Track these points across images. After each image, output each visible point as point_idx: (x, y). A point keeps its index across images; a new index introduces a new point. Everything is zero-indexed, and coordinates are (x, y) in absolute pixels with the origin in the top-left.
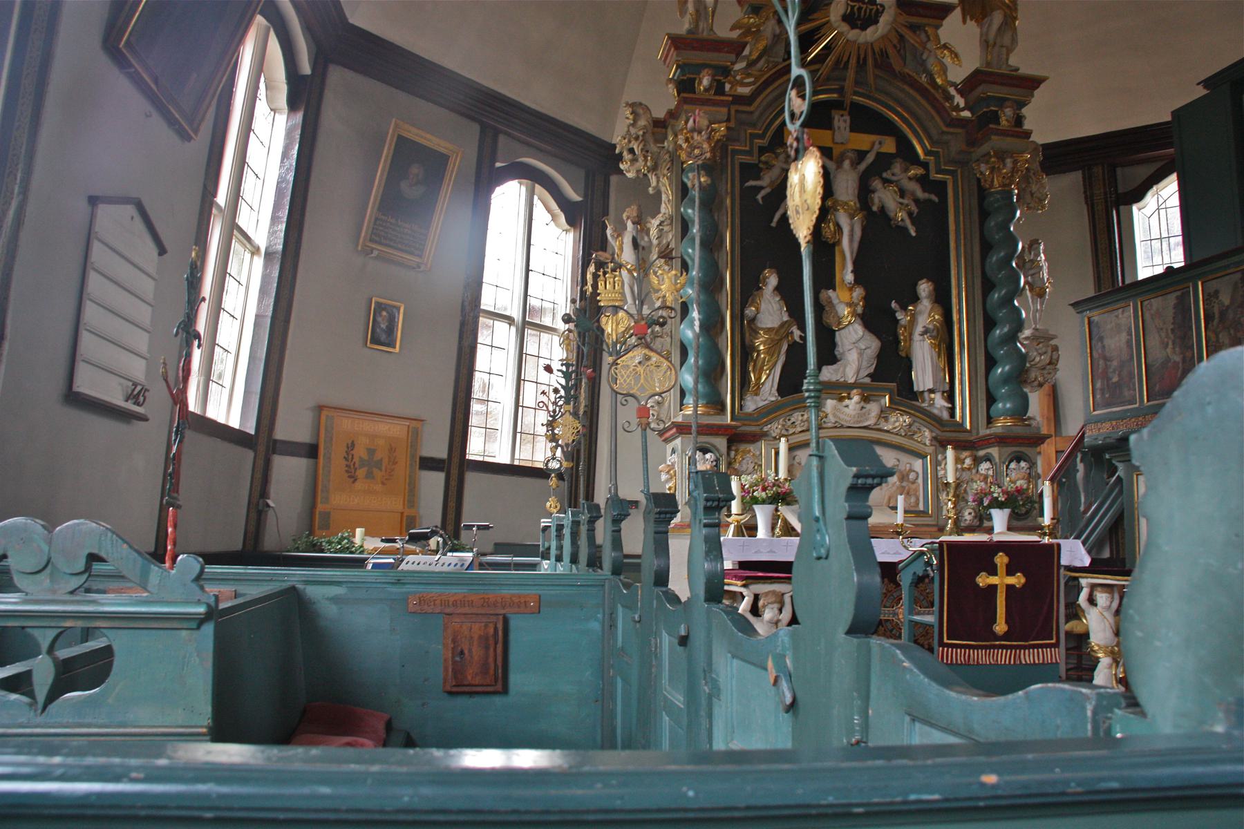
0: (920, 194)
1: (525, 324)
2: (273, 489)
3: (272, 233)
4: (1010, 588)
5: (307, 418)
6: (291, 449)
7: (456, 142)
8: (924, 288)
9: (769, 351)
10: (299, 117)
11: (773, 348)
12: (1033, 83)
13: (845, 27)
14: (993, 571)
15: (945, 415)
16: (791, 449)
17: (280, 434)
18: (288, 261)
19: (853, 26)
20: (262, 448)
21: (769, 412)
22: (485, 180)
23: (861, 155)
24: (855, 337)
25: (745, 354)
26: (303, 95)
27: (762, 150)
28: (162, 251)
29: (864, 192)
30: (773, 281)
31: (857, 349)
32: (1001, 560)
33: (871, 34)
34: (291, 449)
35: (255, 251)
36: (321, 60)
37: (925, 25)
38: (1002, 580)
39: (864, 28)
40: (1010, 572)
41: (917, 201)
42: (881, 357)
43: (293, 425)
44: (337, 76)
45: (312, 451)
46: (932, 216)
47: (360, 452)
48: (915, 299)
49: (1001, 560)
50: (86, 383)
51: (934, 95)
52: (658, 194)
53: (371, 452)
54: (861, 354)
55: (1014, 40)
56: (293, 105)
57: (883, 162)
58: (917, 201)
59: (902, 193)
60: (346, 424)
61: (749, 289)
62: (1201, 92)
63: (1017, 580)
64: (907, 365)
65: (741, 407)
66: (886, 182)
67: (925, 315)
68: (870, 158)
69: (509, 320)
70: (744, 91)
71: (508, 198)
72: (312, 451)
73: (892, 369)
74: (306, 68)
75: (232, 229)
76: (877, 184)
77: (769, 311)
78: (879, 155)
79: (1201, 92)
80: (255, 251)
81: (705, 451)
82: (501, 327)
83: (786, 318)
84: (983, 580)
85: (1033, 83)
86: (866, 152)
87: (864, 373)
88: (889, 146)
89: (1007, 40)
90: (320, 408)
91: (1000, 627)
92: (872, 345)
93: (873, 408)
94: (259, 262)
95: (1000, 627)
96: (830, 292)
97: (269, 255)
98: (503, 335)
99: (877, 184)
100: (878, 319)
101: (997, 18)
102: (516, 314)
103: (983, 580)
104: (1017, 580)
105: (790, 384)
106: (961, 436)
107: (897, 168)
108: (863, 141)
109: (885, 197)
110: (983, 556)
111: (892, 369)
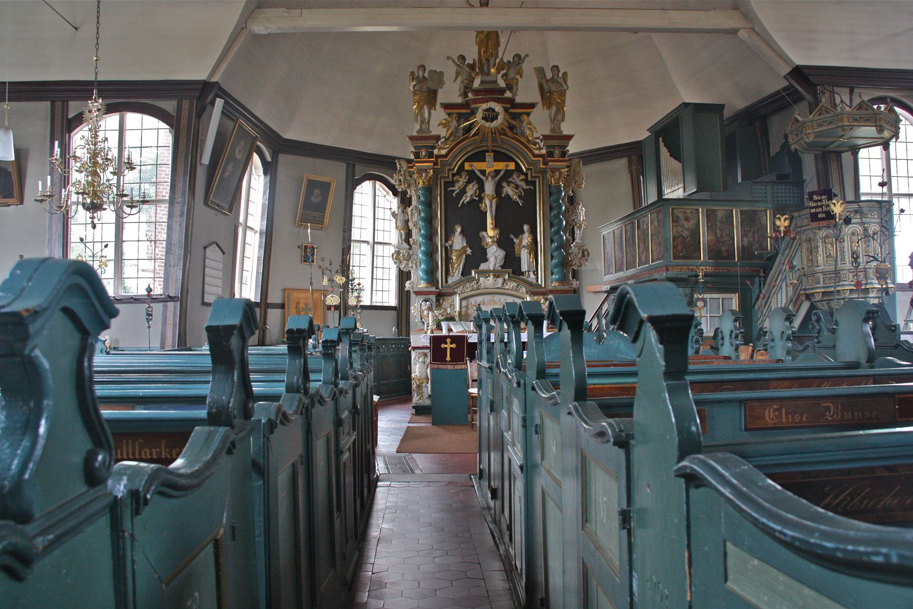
0: (525, 187)
1: (374, 243)
2: (268, 322)
3: (261, 225)
4: (451, 348)
5: (280, 294)
6: (274, 306)
7: (333, 173)
8: (526, 227)
9: (457, 259)
10: (268, 177)
11: (459, 257)
12: (569, 138)
13: (484, 122)
14: (446, 343)
15: (534, 281)
16: (461, 300)
17: (270, 301)
18: (269, 236)
19: (487, 121)
20: (263, 307)
21: (458, 284)
22: (353, 184)
23: (497, 172)
24: (493, 251)
25: (448, 260)
26: (269, 168)
27: (454, 175)
28: (224, 253)
29: (498, 188)
30: (459, 230)
31: (495, 255)
32: (448, 340)
33: (495, 124)
34: (274, 306)
35: (256, 232)
36: (275, 156)
37: (522, 114)
38: (448, 346)
39: (492, 121)
40: (451, 343)
41: (524, 190)
42: (506, 258)
43: (275, 297)
44: (282, 158)
45: (282, 306)
46: (529, 197)
47: (302, 305)
48: (523, 232)
49: (448, 340)
50: (207, 300)
51: (528, 144)
52: (411, 197)
53: (306, 305)
54: (496, 257)
55: (563, 117)
56: (265, 173)
57: (509, 173)
58: (524, 190)
59: (517, 187)
60: (295, 295)
61: (448, 234)
62: (648, 134)
63: (454, 346)
64: (519, 260)
65: (447, 282)
66: (509, 183)
67: (526, 239)
68: (502, 173)
69: (367, 242)
70: (443, 152)
71: (364, 192)
72: (282, 306)
73: (511, 264)
74: (269, 159)
75: (246, 227)
76: (505, 184)
77: (458, 242)
78: (506, 171)
79: (648, 134)
80: (256, 232)
81: (426, 301)
82: (364, 245)
83: (465, 244)
84: (443, 346)
85: (569, 138)
86: (500, 171)
87: (498, 265)
88: (512, 166)
89: (560, 117)
90: (285, 290)
91: (448, 358)
92: (501, 254)
93: (500, 280)
94: (258, 235)
95: (448, 358)
96: (484, 233)
97: (261, 233)
98: (366, 249)
99: (505, 184)
100: (504, 242)
101: (554, 109)
102: (371, 241)
103: (443, 346)
104: (454, 346)
105: (466, 273)
106: (540, 290)
107: (515, 176)
108: (501, 166)
109: (508, 190)
110: (443, 339)
111: (511, 264)
